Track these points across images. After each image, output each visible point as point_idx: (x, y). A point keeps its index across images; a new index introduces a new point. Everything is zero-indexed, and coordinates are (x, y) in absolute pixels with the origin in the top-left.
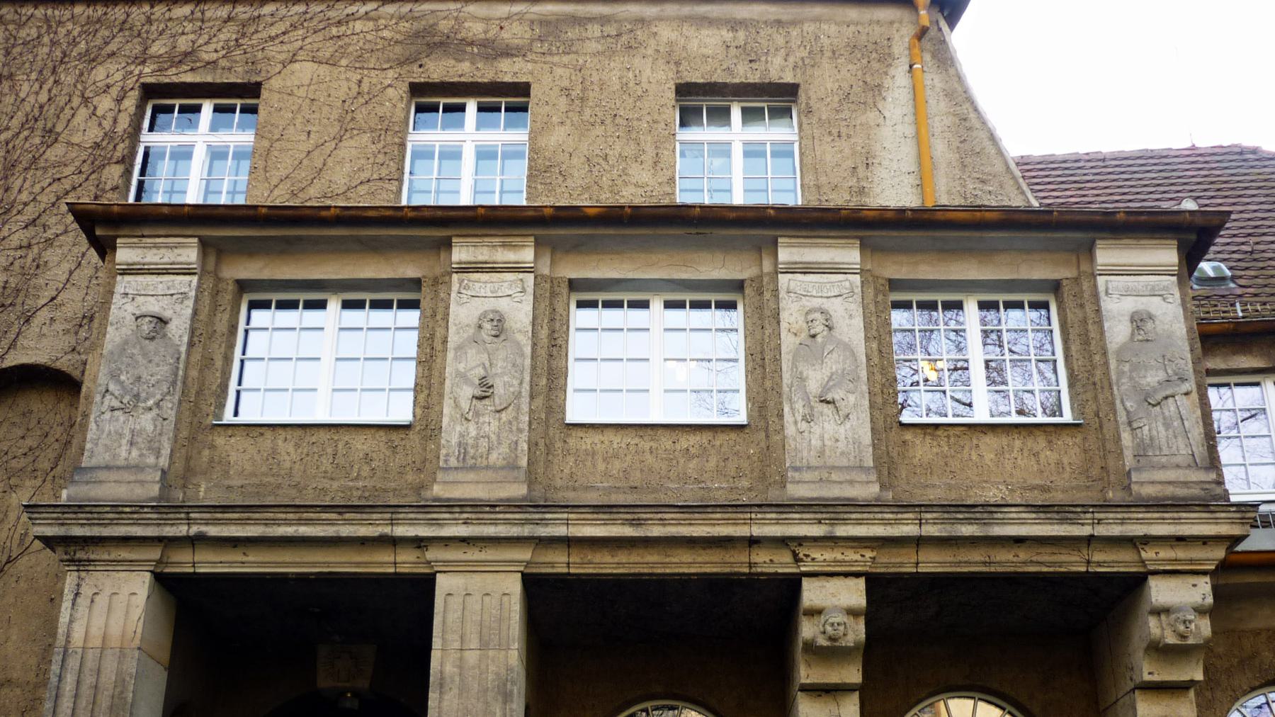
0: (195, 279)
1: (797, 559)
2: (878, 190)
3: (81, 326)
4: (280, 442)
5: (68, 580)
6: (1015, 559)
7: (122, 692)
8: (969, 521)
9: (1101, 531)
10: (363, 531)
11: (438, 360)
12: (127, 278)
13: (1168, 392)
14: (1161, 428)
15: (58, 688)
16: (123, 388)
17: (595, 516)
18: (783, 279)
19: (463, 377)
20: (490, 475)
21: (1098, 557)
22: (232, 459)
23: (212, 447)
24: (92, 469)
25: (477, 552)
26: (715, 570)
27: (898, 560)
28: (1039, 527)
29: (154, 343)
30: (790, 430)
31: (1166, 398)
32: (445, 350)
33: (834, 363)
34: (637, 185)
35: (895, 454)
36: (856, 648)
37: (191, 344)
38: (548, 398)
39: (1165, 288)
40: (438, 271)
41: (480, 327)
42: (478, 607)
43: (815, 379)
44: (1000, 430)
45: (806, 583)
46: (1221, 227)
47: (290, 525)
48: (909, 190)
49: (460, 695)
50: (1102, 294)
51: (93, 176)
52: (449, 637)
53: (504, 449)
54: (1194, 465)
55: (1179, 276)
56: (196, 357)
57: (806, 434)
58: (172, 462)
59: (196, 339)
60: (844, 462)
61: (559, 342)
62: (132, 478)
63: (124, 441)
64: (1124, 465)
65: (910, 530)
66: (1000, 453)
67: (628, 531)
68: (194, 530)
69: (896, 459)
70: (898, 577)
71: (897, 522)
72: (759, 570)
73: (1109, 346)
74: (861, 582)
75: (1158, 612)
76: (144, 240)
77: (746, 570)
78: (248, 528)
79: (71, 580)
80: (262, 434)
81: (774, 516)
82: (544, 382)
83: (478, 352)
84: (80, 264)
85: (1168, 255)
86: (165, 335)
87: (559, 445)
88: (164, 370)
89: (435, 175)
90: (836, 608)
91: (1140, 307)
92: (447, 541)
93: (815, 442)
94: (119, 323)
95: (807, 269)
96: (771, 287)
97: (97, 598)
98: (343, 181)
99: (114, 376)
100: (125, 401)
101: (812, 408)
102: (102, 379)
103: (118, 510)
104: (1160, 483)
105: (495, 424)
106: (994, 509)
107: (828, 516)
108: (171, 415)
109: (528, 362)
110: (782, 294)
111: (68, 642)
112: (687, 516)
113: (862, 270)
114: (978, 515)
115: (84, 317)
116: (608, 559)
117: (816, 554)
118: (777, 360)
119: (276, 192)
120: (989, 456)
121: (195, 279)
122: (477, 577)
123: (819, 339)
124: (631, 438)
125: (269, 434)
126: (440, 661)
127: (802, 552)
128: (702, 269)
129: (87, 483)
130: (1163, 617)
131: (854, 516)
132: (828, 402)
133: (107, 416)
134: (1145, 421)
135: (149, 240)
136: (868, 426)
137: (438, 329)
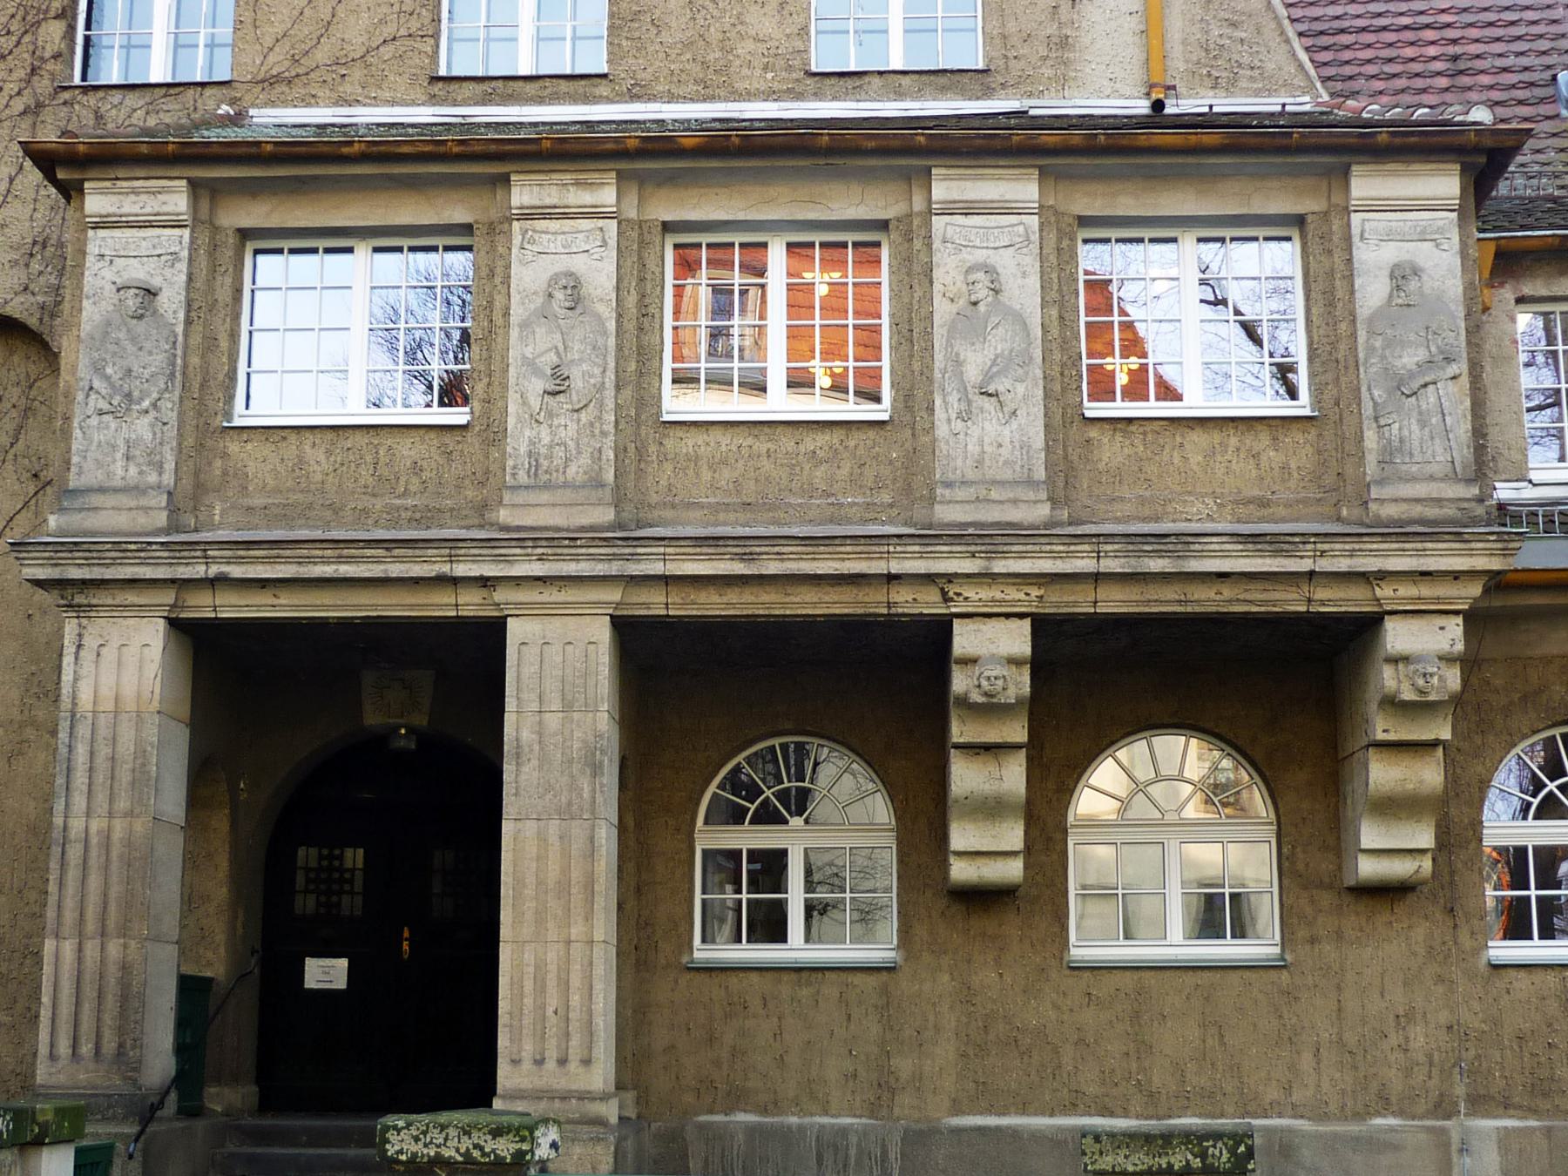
0: (186, 233)
1: (946, 599)
2: (1086, 40)
3: (31, 255)
4: (307, 448)
5: (67, 629)
6: (1218, 597)
7: (144, 765)
8: (1159, 554)
9: (1324, 565)
10: (417, 570)
11: (499, 340)
12: (101, 233)
13: (1427, 379)
14: (1415, 427)
15: (69, 760)
16: (112, 386)
17: (698, 550)
18: (938, 222)
19: (530, 364)
20: (568, 496)
21: (1321, 594)
22: (251, 470)
23: (225, 455)
24: (89, 490)
25: (555, 592)
26: (846, 611)
27: (1071, 599)
28: (1247, 561)
29: (143, 323)
30: (942, 430)
31: (1425, 385)
32: (507, 326)
33: (1000, 341)
34: (756, 39)
35: (1075, 458)
36: (1020, 701)
37: (188, 322)
38: (639, 387)
39: (1440, 230)
40: (494, 214)
41: (550, 295)
42: (559, 659)
43: (975, 363)
44: (1211, 425)
45: (957, 625)
46: (1516, 149)
47: (329, 563)
48: (1130, 39)
49: (540, 767)
50: (1356, 239)
51: (27, 39)
52: (525, 696)
53: (585, 460)
54: (1453, 477)
55: (1462, 211)
56: (196, 339)
57: (961, 436)
58: (178, 479)
59: (193, 314)
60: (1007, 475)
61: (651, 310)
62: (133, 504)
63: (119, 455)
64: (1365, 474)
65: (1085, 565)
66: (1210, 454)
67: (739, 568)
68: (214, 570)
69: (1076, 464)
70: (1071, 619)
71: (1069, 555)
72: (900, 610)
73: (1358, 311)
74: (1026, 624)
75: (1395, 660)
76: (119, 183)
77: (885, 611)
78: (278, 567)
79: (70, 628)
80: (284, 438)
81: (917, 548)
82: (633, 366)
83: (550, 332)
84: (21, 168)
85: (1445, 184)
86: (155, 312)
87: (653, 448)
88: (158, 360)
89: (483, 22)
90: (994, 659)
91: (1406, 257)
92: (518, 581)
93: (973, 448)
94: (97, 296)
95: (969, 209)
96: (923, 233)
97: (104, 651)
98: (360, 40)
99: (98, 369)
100: (115, 403)
101: (969, 402)
102: (84, 371)
103: (120, 549)
104: (1405, 500)
105: (572, 427)
106: (1190, 539)
107: (983, 548)
108: (172, 417)
109: (612, 341)
110: (936, 244)
111: (74, 704)
112: (810, 549)
113: (1041, 207)
114: (1171, 547)
115: (35, 243)
116: (715, 598)
117: (969, 592)
118: (928, 334)
119: (271, 59)
120: (1196, 459)
121: (186, 233)
122: (557, 622)
123: (982, 308)
124: (744, 440)
125: (293, 437)
126: (517, 725)
127: (952, 590)
128: (834, 206)
129: (81, 510)
130: (1401, 666)
131: (1015, 548)
132: (990, 395)
133: (94, 421)
134: (1394, 416)
135: (125, 184)
136: (1040, 422)
137: (497, 297)
